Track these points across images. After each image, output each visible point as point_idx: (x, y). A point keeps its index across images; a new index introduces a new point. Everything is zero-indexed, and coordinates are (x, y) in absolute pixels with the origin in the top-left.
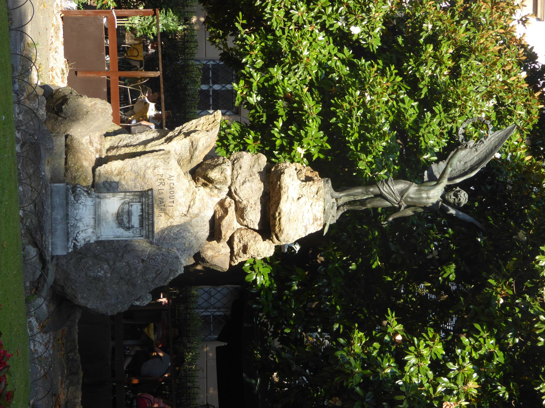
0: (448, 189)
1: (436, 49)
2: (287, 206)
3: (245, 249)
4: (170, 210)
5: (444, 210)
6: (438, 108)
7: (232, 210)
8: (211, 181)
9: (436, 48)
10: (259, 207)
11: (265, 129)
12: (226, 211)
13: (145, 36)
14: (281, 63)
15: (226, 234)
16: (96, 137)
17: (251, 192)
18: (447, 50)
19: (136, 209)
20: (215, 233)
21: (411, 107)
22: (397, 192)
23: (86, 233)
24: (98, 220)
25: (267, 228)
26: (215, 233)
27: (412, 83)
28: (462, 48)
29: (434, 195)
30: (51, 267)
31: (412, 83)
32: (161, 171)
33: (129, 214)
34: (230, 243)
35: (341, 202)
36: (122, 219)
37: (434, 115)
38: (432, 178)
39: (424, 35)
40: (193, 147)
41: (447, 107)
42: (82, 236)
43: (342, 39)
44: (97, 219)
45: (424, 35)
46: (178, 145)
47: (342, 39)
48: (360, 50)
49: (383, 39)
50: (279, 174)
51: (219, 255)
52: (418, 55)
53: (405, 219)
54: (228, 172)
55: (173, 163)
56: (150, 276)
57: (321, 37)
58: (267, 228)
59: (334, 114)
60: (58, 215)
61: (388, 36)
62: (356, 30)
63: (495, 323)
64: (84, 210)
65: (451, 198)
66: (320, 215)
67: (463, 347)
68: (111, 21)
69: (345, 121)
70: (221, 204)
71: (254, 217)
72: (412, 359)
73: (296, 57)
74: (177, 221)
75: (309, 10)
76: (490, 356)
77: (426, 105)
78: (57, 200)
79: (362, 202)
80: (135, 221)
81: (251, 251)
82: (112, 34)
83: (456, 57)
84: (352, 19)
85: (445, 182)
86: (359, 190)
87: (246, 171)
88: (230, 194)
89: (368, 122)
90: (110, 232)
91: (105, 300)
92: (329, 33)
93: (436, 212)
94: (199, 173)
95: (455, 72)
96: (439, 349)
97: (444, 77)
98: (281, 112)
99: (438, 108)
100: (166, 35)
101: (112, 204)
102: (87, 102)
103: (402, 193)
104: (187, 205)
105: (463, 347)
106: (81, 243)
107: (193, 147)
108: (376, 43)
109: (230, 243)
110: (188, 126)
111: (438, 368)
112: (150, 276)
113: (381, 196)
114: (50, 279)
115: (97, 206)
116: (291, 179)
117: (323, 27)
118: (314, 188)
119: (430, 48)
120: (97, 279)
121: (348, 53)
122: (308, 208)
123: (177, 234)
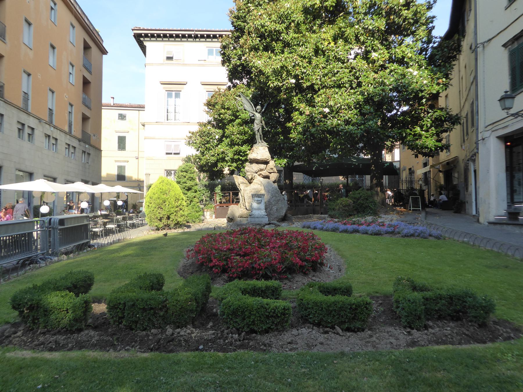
0: (256, 111)
1: (222, 114)
2: (259, 157)
3: (272, 169)
4: (259, 190)
5: (263, 113)
6: (238, 114)
7: (260, 172)
8: (252, 178)
9: (222, 114)
10: (260, 165)
11: (240, 162)
12: (261, 174)
13: (222, 196)
14: (225, 157)
15: (268, 174)
16: (241, 210)
17: (256, 167)
18: (223, 111)
19: (256, 199)
20: (267, 177)
21: (238, 121)
22: (257, 126)
23: (263, 212)
24: (259, 209)
25: (266, 163)
26: (267, 177)
27: (232, 121)
28: (222, 107)
29: (258, 116)
30: (272, 222)
31: (232, 121)
32: (248, 192)
33: (257, 201)
34: (270, 173)
35: (260, 141)
36: (259, 202)
37: (240, 115)
38: (253, 116)
39: (218, 118)
40: (243, 183)
41: (238, 111)
42: (263, 214)
43: (220, 141)
44: (259, 210)
45: (218, 118)
46: (242, 187)
47: (220, 141)
48: (223, 136)
49: (220, 129)
50: (251, 159)
51: (274, 176)
52: (223, 119)
53: (266, 124)
54: (249, 173)
55: (246, 188)
56: (277, 195)
57: (219, 146)
58: (266, 163)
59: (238, 143)
60: (257, 220)
61: (219, 128)
62: (217, 137)
63: (290, 98)
64: (256, 213)
65: (259, 111)
66: (263, 148)
67: (296, 106)
68: (218, 205)
69: (240, 140)
70: (259, 175)
71: (263, 166)
72: (299, 121)
73: (223, 153)
74: (263, 188)
75: (212, 149)
76: (299, 99)
77: (237, 117)
78: (253, 220)
79: (260, 136)
80: (260, 199)
81: (273, 167)
82: (221, 205)
83: (224, 109)
84: (214, 138)
85: (255, 112)
86: (256, 137)
87: (249, 168)
88: (256, 173)
89: (240, 133)
90: (262, 206)
91: (283, 208)
92: (219, 144)
93: (263, 114)
94: (250, 182)
95: (228, 109)
96: (297, 113)
97: (230, 112)
98: (238, 157)
99: (238, 114)
100: (222, 190)
101: (255, 205)
102: (229, 212)
103: (257, 124)
104: (259, 184)
105: (296, 106)
106: (265, 214)
107: (243, 183)
108: (221, 131)
109: (270, 173)
110: (237, 185)
111: (301, 114)
112: (277, 195)
113: (258, 130)
114: (275, 222)
115: (255, 209)
116: (252, 156)
117: (217, 146)
118: (255, 149)
119: (222, 116)
120: (277, 210)
121: (224, 139)
122: (261, 151)
123: (266, 187)
